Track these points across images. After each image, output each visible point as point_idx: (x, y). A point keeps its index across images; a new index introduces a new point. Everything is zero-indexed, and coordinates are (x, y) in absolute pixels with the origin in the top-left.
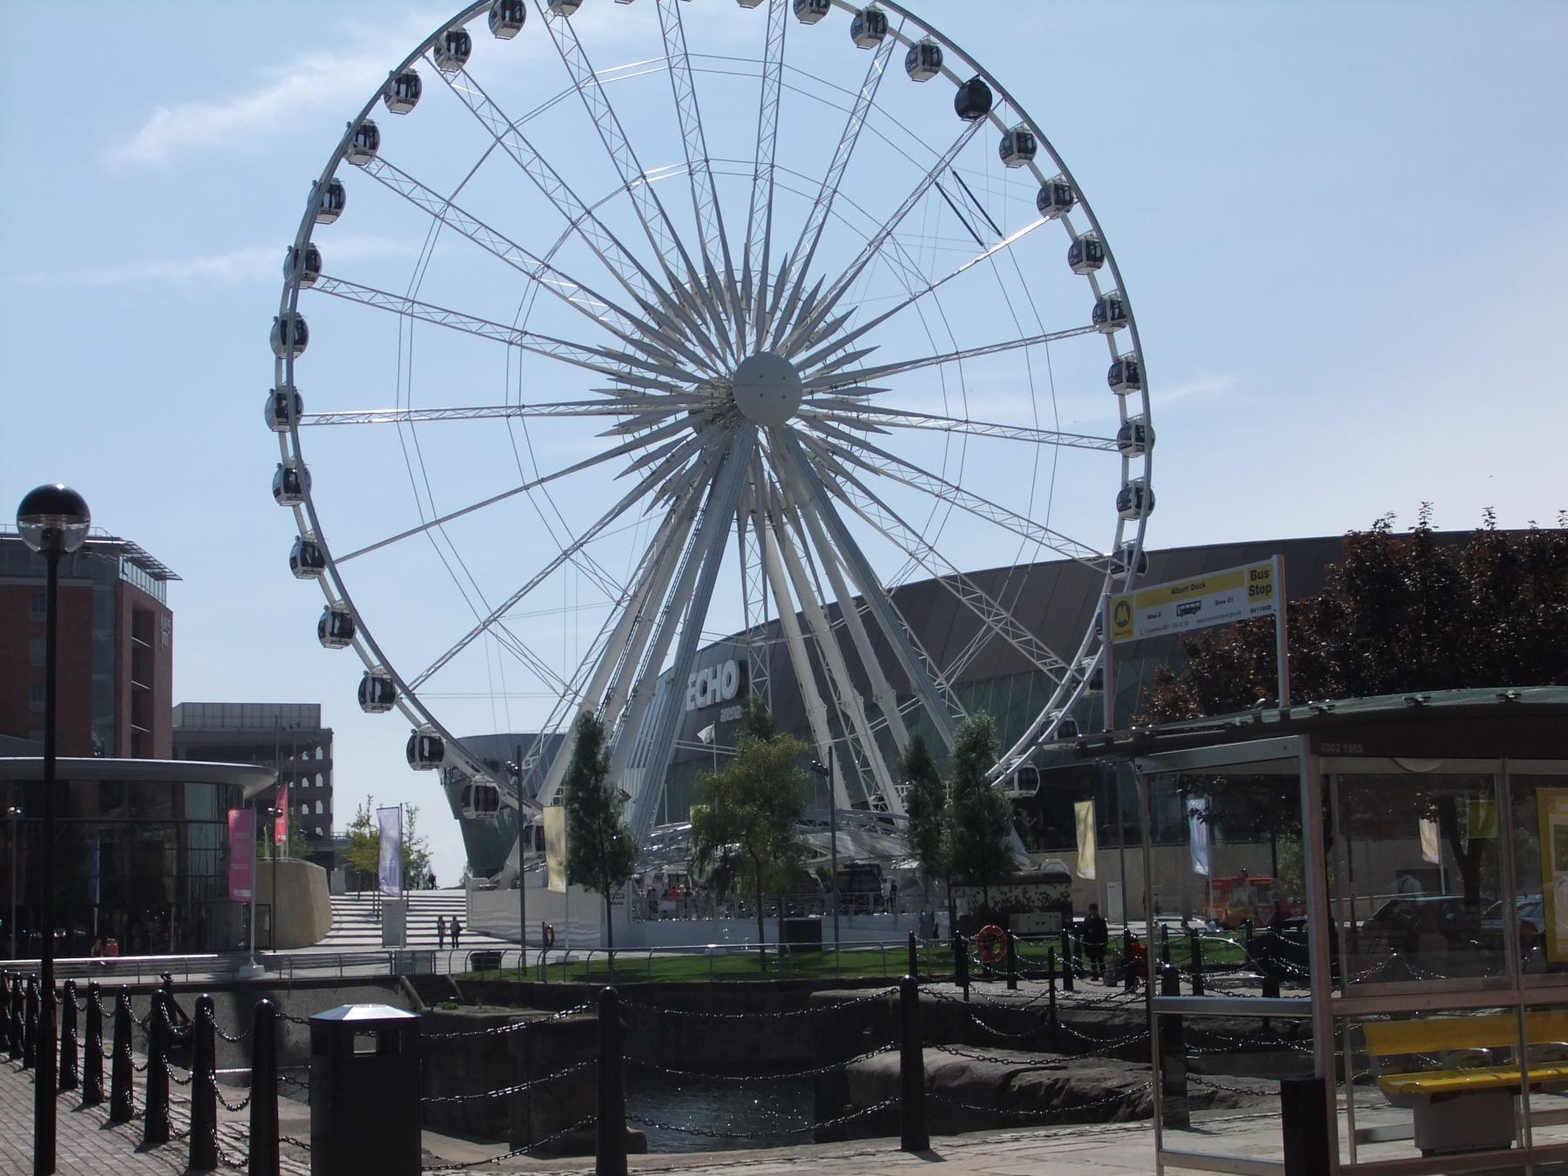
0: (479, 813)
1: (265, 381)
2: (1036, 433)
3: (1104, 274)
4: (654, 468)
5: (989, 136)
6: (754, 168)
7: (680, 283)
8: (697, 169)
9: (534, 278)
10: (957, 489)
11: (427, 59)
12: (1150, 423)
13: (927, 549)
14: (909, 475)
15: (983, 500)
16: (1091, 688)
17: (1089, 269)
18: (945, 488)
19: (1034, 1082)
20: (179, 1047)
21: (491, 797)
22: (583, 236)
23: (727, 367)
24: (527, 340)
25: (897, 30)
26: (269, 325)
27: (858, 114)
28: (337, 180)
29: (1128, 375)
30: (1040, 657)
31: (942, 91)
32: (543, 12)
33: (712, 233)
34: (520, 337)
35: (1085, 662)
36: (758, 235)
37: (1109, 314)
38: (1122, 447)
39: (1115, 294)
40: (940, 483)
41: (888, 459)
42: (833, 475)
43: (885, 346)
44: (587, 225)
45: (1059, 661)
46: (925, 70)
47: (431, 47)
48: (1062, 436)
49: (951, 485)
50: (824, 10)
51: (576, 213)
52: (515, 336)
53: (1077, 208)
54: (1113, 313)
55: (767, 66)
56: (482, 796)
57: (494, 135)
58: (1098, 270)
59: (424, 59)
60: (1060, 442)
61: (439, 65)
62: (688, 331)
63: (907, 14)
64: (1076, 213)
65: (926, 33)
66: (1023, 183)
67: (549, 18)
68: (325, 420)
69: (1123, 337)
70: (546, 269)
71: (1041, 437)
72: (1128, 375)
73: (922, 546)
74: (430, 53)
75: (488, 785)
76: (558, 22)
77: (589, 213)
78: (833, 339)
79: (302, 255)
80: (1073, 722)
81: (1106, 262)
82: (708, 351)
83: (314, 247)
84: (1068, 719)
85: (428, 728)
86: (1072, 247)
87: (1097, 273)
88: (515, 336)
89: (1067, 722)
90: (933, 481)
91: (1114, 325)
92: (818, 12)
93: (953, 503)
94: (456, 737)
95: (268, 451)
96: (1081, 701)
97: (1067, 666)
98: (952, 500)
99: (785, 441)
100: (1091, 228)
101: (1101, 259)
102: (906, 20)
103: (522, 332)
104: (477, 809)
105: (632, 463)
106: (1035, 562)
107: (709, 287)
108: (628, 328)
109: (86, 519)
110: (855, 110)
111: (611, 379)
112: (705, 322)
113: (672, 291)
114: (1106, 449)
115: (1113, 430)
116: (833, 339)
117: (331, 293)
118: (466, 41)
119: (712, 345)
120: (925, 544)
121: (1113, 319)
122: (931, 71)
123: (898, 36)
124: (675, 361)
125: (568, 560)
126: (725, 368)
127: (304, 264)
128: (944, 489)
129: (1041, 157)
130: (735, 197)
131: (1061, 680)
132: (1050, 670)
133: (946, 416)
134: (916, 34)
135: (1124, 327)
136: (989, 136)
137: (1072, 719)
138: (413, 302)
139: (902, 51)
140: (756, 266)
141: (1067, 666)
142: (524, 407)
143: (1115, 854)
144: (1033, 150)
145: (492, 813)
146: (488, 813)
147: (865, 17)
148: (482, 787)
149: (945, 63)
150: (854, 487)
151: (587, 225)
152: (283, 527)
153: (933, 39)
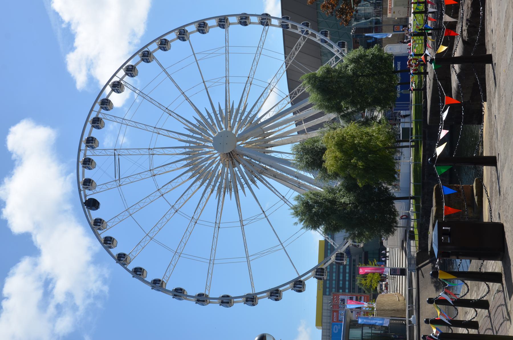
0: (344, 260)
1: (192, 304)
2: (257, 54)
3: (210, 23)
4: (245, 183)
5: (159, 54)
6: (156, 133)
7: (187, 164)
8: (152, 152)
9: (177, 211)
10: (248, 77)
11: (101, 233)
12: (260, 15)
13: (287, 97)
14: (245, 94)
15: (275, 76)
16: (327, 36)
17: (207, 27)
18: (248, 82)
19: (467, 32)
20: (449, 228)
21: (320, 270)
22: (180, 208)
23: (216, 153)
24: (218, 222)
25: (120, 79)
26: (175, 300)
27: (145, 96)
28: (133, 269)
29: (244, 20)
30: (300, 45)
31: (142, 67)
32: (93, 193)
33: (173, 151)
34: (194, 220)
35: (318, 38)
36: (177, 136)
37: (223, 23)
38: (267, 25)
39: (217, 20)
40: (247, 84)
41: (241, 102)
42: (242, 120)
43: (219, 100)
44: (163, 191)
45: (301, 38)
46: (134, 71)
47: (97, 231)
48: (260, 46)
49: (268, 86)
50: (109, 101)
51: (158, 194)
52: (194, 221)
53: (187, 28)
54: (223, 22)
55: (123, 123)
56: (339, 258)
57: (108, 221)
58: (208, 24)
59: (101, 234)
60: (261, 47)
61: (104, 229)
62: (202, 164)
63: (115, 75)
64: (189, 29)
65: (122, 69)
66: (176, 45)
67: (95, 192)
68: (208, 286)
69: (231, 20)
70: (174, 207)
71: (259, 53)
72: (244, 20)
73: (286, 99)
74: (99, 232)
75: (335, 256)
76: (97, 189)
77: (159, 190)
78: (214, 117)
79: (154, 285)
80: (338, 43)
81: (207, 22)
82: (209, 159)
83: (152, 281)
84: (337, 45)
85: (313, 272)
86: (199, 32)
87: (209, 25)
88: (194, 221)
89: (338, 45)
90: (247, 86)
91: (227, 22)
92: (109, 103)
93: (274, 87)
94: (318, 264)
95: (215, 308)
96: (331, 39)
97: (335, 56)
98: (273, 87)
99: (243, 137)
100: (194, 25)
101: (204, 23)
102: (116, 75)
103: (192, 218)
104: (343, 260)
105: (242, 190)
106: (284, 54)
107: (189, 155)
108: (198, 183)
109: (265, 335)
110: (143, 97)
111: (186, 129)
112: (200, 158)
113: (188, 167)
114: (267, 32)
115: (262, 27)
116: (214, 117)
117: (169, 278)
118: (97, 220)
119: (209, 157)
120: (285, 98)
121: (224, 22)
122: (134, 69)
123: (122, 79)
124: (209, 172)
125: (243, 222)
126: (216, 154)
127: (157, 284)
128: (249, 82)
129: (168, 38)
130: (164, 141)
131: (306, 37)
132: (304, 41)
133: (245, 84)
134: (122, 73)
135: (228, 18)
136: (159, 54)
137: (337, 43)
138: (176, 252)
139: (127, 79)
140: (185, 138)
141: (335, 56)
142: (216, 222)
143: (384, 28)
144: (165, 40)
145: (325, 270)
146: (344, 257)
147: (114, 88)
148: (336, 258)
149: (133, 64)
150: (262, 118)
151: (163, 191)
152: (240, 307)
153: (124, 67)
